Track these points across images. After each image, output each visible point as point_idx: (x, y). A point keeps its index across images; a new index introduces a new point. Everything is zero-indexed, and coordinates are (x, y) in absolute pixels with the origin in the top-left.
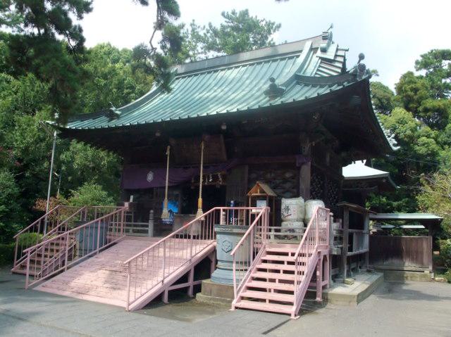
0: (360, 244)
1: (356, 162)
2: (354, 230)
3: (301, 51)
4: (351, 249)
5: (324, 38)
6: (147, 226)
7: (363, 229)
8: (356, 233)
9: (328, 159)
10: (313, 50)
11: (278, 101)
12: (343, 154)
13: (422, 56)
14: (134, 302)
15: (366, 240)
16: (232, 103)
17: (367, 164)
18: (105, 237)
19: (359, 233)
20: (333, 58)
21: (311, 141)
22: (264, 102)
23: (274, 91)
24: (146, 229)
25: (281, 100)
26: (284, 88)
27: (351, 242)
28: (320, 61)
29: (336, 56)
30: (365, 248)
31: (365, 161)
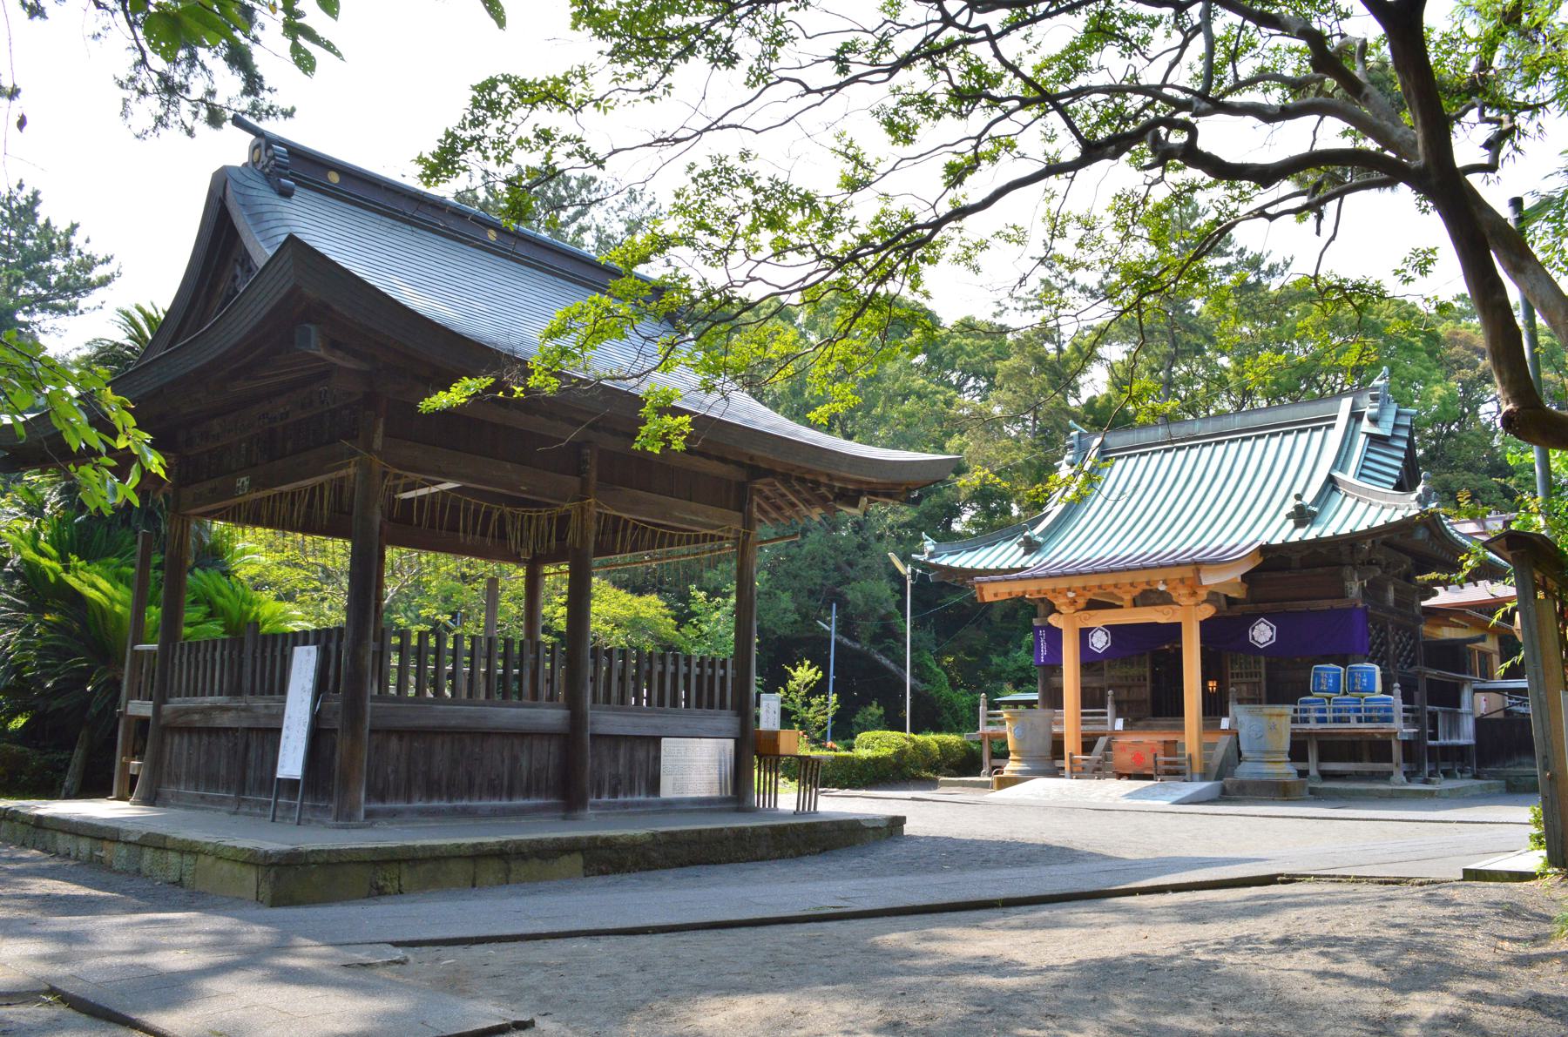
0: (1454, 728)
4: (1434, 737)
9: (1391, 595)
23: (1302, 516)
27: (1434, 726)
29: (1396, 426)
30: (1466, 735)
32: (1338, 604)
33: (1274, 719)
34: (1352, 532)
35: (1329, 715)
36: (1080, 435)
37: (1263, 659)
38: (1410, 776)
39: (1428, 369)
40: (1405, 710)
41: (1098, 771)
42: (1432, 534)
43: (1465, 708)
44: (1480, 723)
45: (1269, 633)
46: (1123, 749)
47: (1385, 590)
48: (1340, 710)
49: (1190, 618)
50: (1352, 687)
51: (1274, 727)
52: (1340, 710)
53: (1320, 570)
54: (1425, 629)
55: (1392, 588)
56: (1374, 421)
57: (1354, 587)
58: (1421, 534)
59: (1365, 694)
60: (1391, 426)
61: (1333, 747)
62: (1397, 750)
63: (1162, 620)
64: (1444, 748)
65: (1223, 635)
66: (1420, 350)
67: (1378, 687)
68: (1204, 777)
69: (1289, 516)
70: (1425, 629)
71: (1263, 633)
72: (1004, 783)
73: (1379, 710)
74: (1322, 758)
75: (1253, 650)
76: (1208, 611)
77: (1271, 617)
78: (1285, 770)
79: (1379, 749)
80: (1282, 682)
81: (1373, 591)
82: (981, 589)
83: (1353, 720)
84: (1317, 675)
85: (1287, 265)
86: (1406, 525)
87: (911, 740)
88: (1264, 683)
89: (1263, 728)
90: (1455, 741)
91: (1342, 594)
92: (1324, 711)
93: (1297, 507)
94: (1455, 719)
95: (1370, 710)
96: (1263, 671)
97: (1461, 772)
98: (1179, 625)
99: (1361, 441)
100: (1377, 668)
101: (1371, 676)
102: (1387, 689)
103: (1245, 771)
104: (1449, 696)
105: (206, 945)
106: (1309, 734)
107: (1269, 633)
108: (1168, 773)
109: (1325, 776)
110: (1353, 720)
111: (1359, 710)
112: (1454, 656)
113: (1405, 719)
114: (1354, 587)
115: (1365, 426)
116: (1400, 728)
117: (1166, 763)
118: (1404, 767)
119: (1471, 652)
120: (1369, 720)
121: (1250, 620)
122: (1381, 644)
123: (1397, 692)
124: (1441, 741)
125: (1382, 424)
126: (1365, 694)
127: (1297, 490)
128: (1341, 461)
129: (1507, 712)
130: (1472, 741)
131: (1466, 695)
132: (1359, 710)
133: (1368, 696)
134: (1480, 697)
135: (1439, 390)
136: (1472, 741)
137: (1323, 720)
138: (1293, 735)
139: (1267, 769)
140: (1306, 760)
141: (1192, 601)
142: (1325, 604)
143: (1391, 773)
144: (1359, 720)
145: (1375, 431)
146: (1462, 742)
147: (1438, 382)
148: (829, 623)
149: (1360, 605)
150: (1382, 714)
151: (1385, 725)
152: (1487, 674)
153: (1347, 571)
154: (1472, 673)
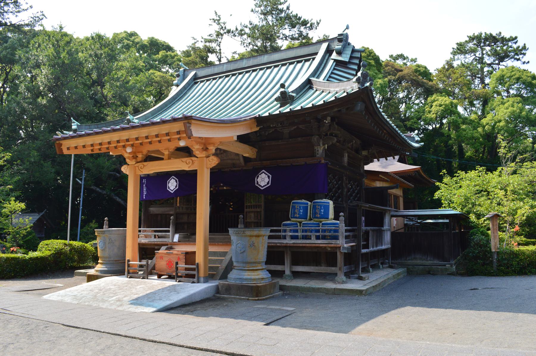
0: (379, 239)
1: (380, 159)
2: (368, 228)
3: (316, 54)
4: (366, 246)
5: (340, 40)
6: (168, 231)
7: (383, 227)
8: (373, 230)
9: (346, 159)
10: (329, 51)
11: (286, 109)
12: (364, 153)
13: (457, 44)
14: (252, 212)
15: (387, 237)
16: (259, 309)
17: (400, 161)
18: (244, 215)
19: (377, 230)
20: (347, 60)
21: (324, 144)
22: (275, 109)
23: (285, 99)
24: (168, 234)
25: (291, 107)
26: (294, 95)
27: (367, 240)
28: (335, 63)
29: (351, 58)
30: (386, 244)
31: (397, 157)
32: (310, 161)
33: (254, 239)
34: (314, 106)
35: (300, 234)
36: (184, 70)
37: (263, 196)
38: (348, 275)
39: (376, 73)
40: (346, 231)
41: (149, 272)
42: (367, 108)
43: (386, 227)
44: (394, 235)
45: (267, 180)
46: (162, 258)
47: (343, 156)
48: (306, 231)
49: (203, 167)
50: (314, 215)
51: (253, 245)
52: (306, 231)
53: (299, 139)
54: (366, 181)
55: (346, 155)
56: (339, 53)
57: (320, 150)
58: (360, 106)
59: (324, 220)
60: (349, 56)
61: (302, 256)
62: (340, 259)
63: (186, 168)
64: (373, 253)
65: (231, 183)
66: (374, 66)
67: (331, 215)
68: (209, 277)
69: (276, 100)
70: (366, 181)
71: (263, 180)
72: (91, 278)
73: (330, 231)
74: (295, 263)
75: (257, 190)
76: (214, 161)
77: (269, 170)
78: (259, 276)
79: (328, 257)
80: (273, 214)
81: (330, 152)
82: (61, 145)
83: (313, 238)
84: (294, 207)
85: (318, 24)
86: (350, 98)
87: (70, 245)
88: (263, 213)
89: (249, 245)
90: (379, 248)
91: (313, 155)
92: (297, 231)
93: (282, 93)
94: (379, 235)
95: (324, 231)
96: (263, 204)
97: (382, 264)
98: (196, 170)
99: (331, 62)
100: (331, 203)
101: (327, 208)
102: (336, 217)
103: (234, 276)
104: (376, 220)
105: (113, 263)
106: (286, 247)
107: (267, 180)
108: (188, 276)
109: (296, 275)
110: (313, 238)
111: (318, 231)
112: (381, 197)
113: (347, 237)
114: (320, 150)
115: (334, 56)
116: (343, 244)
117: (186, 269)
118: (345, 269)
119: (390, 195)
120: (324, 238)
121: (256, 173)
122: (338, 188)
123: (342, 218)
124: (371, 249)
125: (343, 55)
126: (324, 220)
127: (282, 82)
128: (317, 73)
129: (406, 225)
130: (389, 246)
131: (387, 219)
132: (318, 231)
133: (325, 221)
134: (394, 220)
135: (380, 81)
136: (389, 246)
137: (296, 237)
138: (269, 247)
139: (247, 275)
140: (283, 264)
141: (204, 154)
142: (301, 161)
143: (336, 274)
144: (318, 238)
145: (339, 58)
146: (384, 247)
147: (380, 79)
148: (81, 180)
149: (323, 161)
150: (332, 233)
151: (333, 241)
152: (397, 207)
153: (315, 139)
154: (390, 206)
